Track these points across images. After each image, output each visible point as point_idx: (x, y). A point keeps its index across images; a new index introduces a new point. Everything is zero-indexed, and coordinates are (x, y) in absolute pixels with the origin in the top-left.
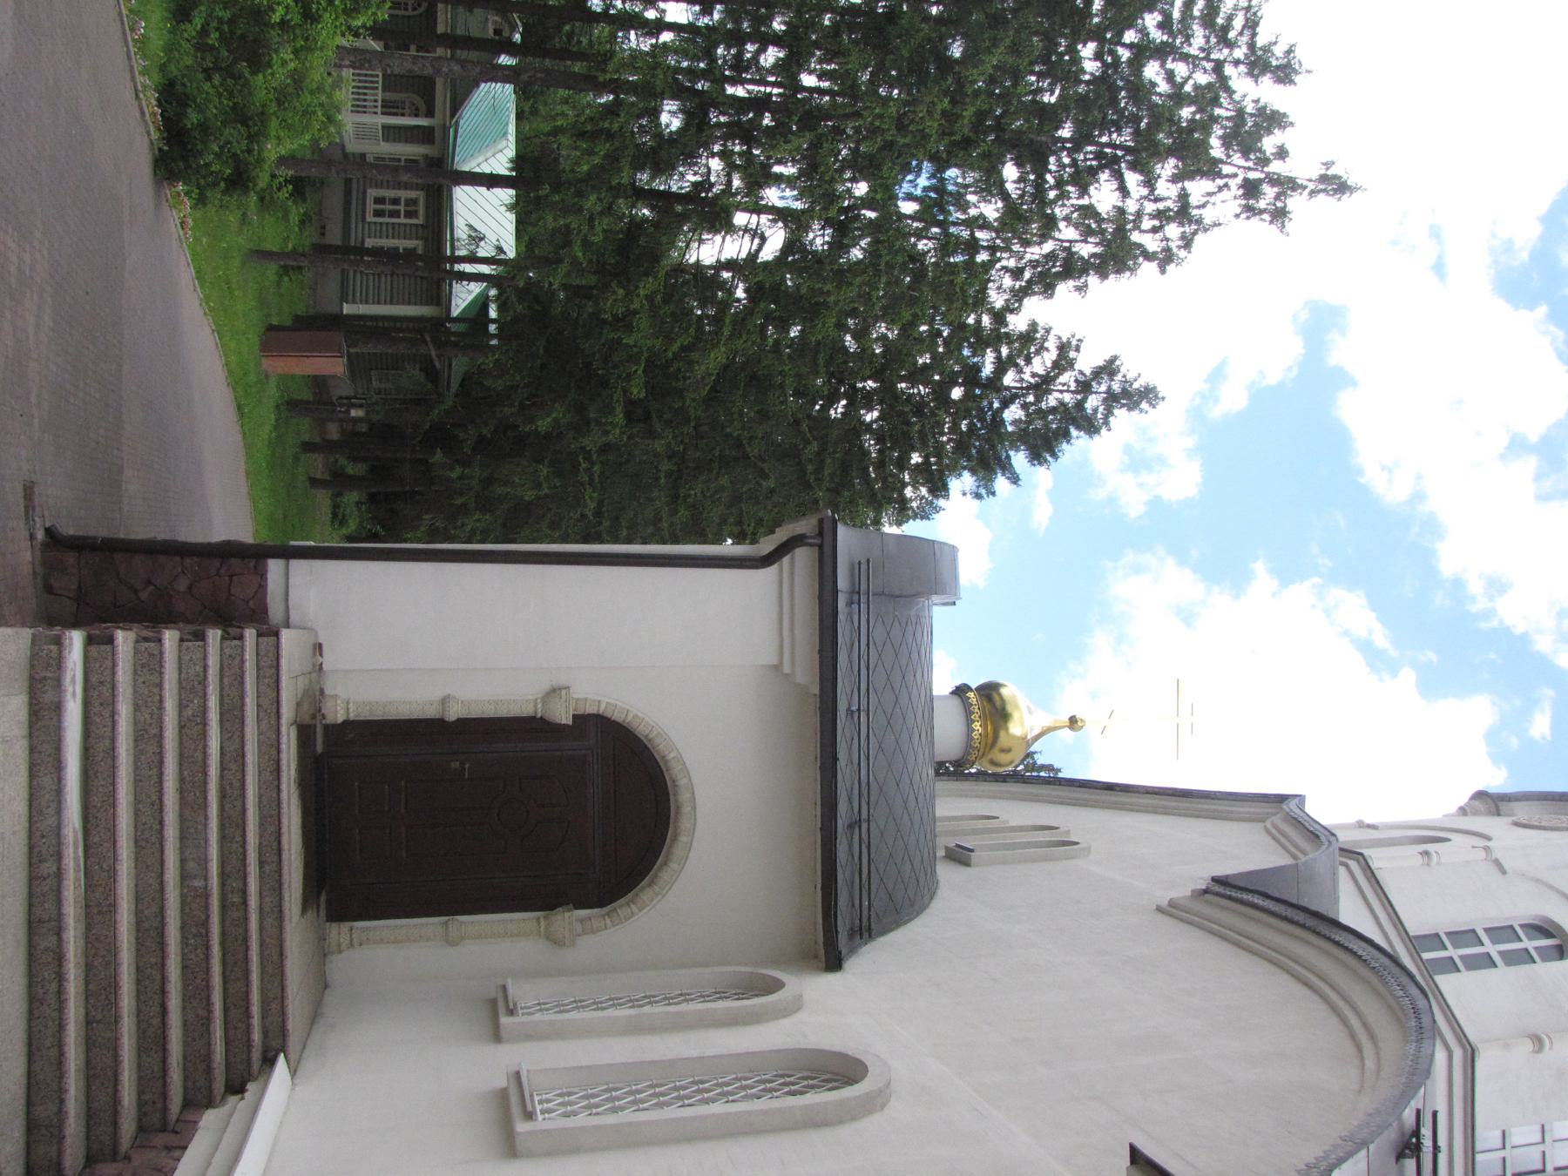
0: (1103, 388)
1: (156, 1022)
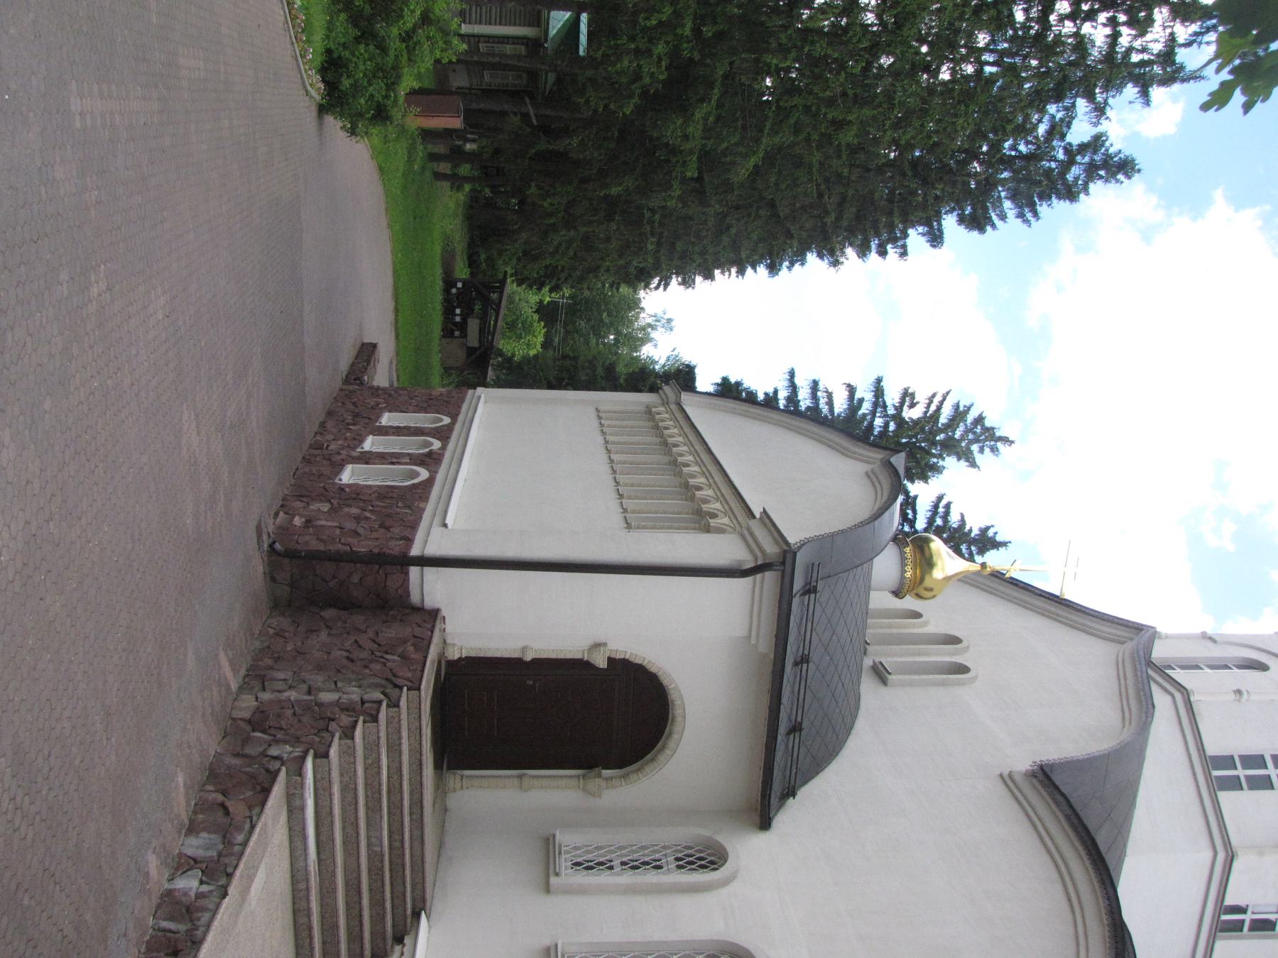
0: (1087, 159)
1: (357, 929)
